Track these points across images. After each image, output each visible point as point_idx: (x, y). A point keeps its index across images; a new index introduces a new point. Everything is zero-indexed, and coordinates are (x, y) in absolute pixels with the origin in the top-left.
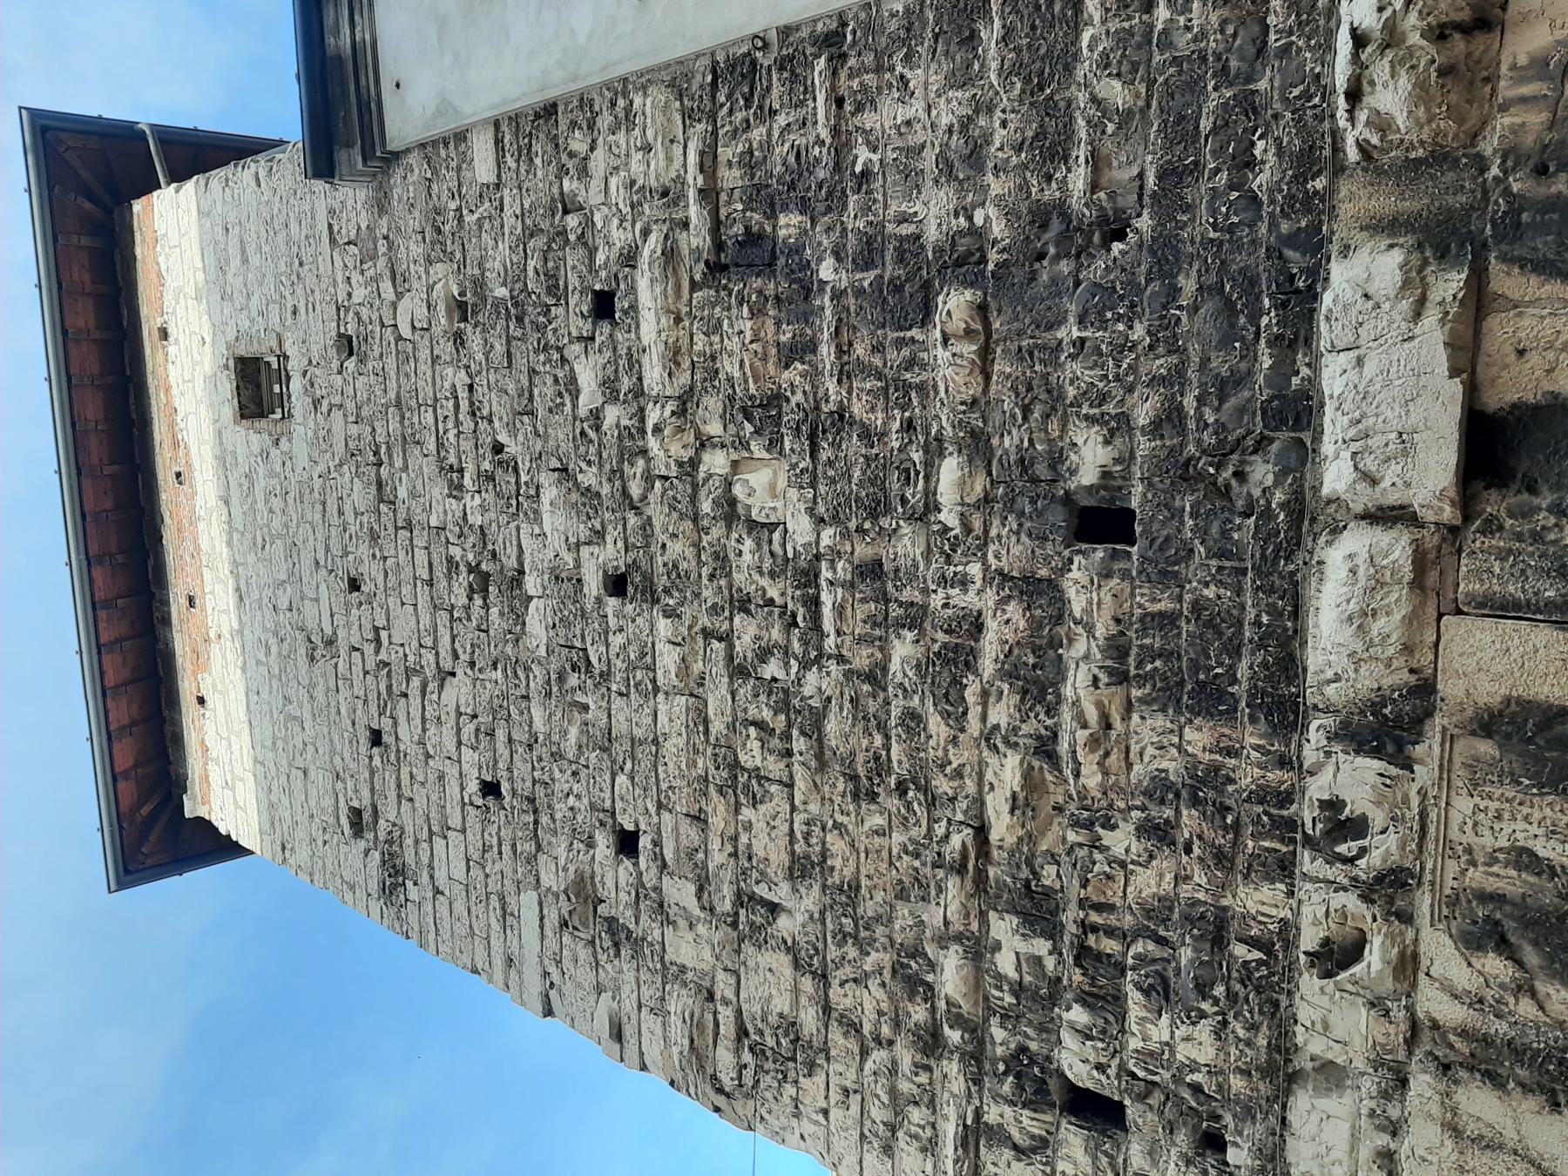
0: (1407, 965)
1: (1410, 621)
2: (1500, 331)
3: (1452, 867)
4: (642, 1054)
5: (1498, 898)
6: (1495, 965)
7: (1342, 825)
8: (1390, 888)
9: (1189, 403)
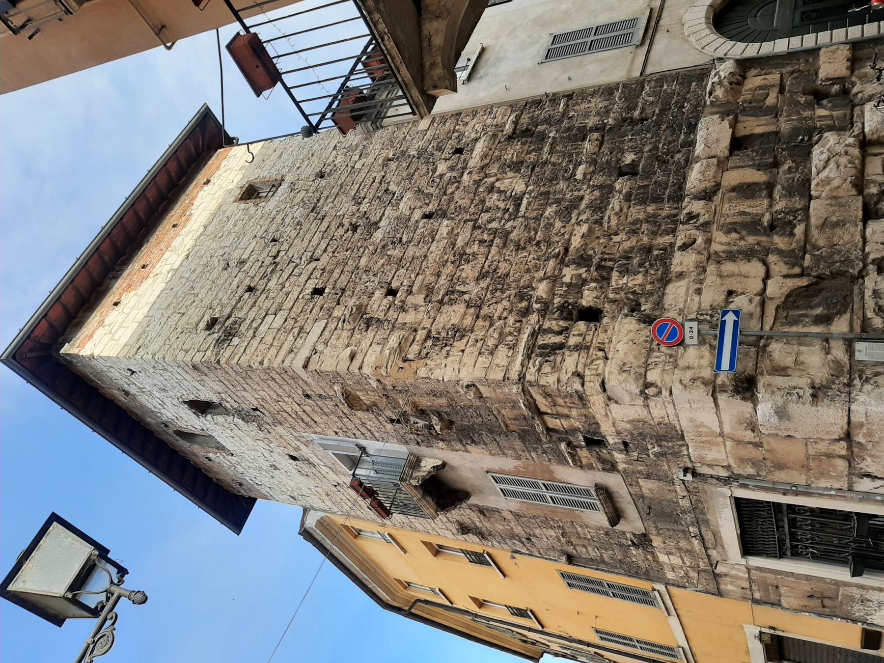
0: (709, 241)
1: (716, 172)
2: (740, 126)
3: (722, 219)
4: (363, 362)
5: (736, 223)
6: (734, 235)
7: (691, 217)
8: (705, 226)
9: (661, 146)
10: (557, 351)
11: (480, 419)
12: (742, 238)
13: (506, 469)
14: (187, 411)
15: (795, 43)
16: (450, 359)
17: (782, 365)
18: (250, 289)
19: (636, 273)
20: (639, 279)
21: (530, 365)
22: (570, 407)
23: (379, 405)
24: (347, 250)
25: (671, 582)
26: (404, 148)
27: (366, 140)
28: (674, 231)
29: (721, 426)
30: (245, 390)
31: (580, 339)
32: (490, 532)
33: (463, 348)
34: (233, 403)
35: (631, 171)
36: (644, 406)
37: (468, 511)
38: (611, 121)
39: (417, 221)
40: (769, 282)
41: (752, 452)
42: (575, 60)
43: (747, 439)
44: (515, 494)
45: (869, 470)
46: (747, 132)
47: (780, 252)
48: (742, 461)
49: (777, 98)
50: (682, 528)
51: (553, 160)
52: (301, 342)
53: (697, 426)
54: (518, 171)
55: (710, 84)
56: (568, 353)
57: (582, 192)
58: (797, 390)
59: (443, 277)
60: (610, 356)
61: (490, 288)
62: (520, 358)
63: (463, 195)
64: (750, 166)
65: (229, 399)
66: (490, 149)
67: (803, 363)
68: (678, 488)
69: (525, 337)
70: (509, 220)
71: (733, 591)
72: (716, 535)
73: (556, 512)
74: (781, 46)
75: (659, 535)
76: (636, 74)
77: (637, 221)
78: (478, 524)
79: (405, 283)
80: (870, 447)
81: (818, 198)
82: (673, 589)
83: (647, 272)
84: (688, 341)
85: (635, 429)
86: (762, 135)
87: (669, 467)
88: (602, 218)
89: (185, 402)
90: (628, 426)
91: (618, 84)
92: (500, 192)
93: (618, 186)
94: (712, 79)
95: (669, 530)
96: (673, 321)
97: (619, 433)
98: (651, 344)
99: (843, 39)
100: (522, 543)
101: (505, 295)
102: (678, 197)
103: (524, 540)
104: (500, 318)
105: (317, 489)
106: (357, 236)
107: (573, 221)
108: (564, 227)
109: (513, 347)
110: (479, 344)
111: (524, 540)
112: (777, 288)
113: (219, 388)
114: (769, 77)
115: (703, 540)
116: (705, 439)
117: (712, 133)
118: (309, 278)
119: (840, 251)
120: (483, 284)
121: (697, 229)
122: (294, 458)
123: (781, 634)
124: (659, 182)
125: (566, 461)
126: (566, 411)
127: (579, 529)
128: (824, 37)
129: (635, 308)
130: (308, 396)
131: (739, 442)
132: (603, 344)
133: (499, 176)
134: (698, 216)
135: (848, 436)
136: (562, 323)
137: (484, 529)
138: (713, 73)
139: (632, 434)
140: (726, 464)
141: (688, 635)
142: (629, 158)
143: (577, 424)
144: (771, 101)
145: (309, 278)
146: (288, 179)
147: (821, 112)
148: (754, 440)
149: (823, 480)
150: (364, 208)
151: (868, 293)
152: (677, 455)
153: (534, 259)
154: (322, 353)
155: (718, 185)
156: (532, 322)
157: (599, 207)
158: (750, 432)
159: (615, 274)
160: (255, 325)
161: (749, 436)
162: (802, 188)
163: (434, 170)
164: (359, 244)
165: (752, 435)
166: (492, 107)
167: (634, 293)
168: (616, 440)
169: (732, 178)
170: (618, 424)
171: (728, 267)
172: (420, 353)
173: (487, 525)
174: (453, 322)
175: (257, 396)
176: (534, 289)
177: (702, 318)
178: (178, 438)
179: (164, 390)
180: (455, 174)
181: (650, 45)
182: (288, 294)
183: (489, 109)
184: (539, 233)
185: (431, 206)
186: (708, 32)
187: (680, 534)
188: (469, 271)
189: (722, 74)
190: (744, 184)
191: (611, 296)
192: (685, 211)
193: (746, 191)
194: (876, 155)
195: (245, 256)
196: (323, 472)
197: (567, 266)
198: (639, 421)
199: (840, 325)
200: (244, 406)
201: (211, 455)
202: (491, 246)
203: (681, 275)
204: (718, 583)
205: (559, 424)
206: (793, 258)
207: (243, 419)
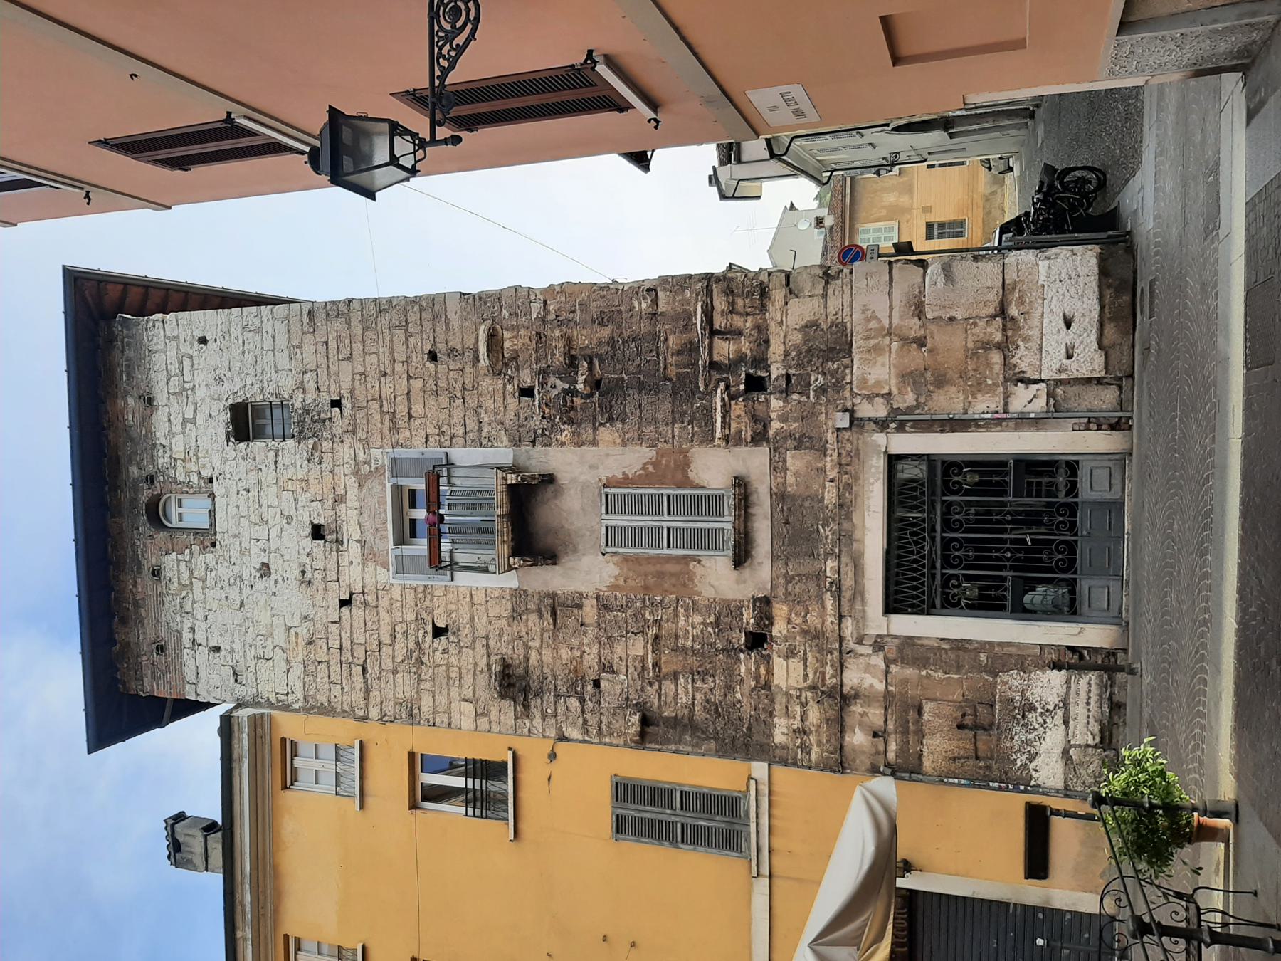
29: (890, 317)
135: (1002, 312)
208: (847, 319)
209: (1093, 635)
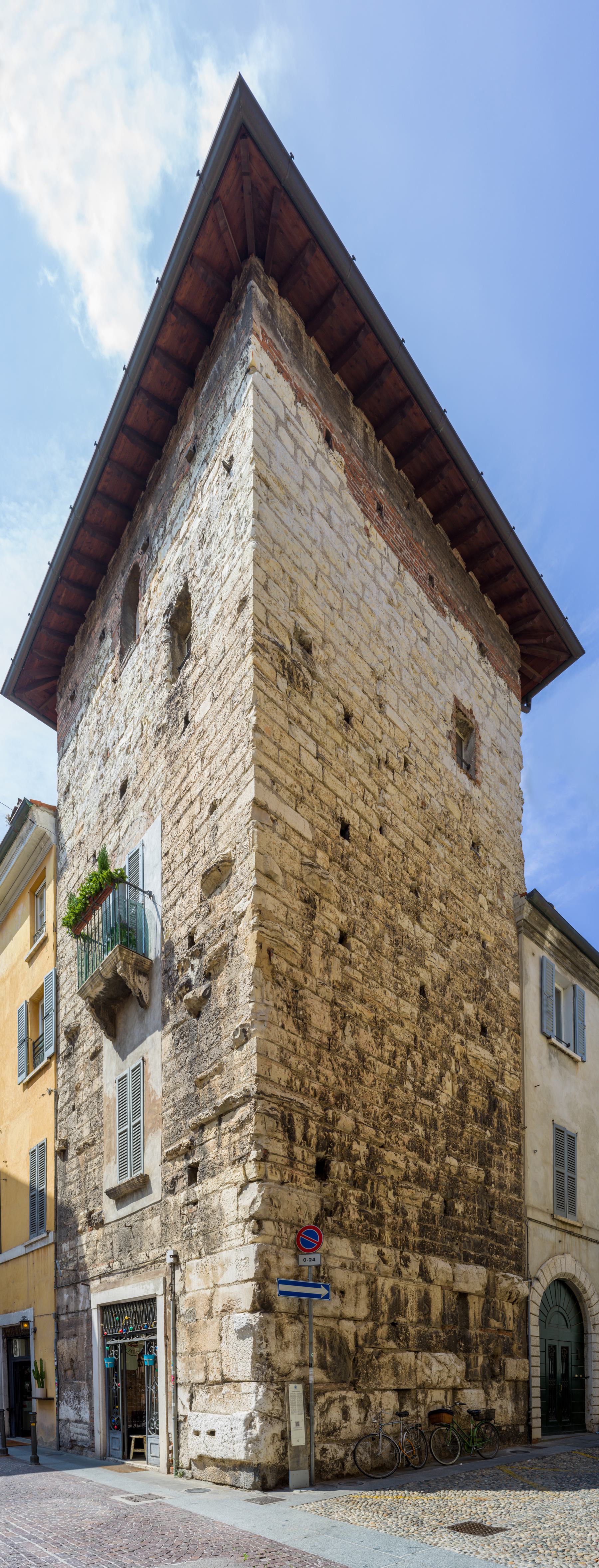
4: (266, 892)
5: (399, 1296)
6: (389, 1295)
7: (406, 1260)
9: (467, 1234)
10: (287, 1134)
11: (205, 1048)
12: (387, 1300)
13: (150, 1081)
14: (173, 590)
15: (535, 1341)
16: (274, 1012)
17: (284, 1332)
18: (348, 717)
19: (360, 1211)
20: (355, 1216)
21: (272, 1105)
22: (229, 1148)
23: (211, 917)
24: (391, 876)
25: (59, 1247)
26: (496, 962)
27: (508, 912)
28: (395, 1245)
29: (224, 1285)
30: (214, 699)
31: (300, 1158)
32: (74, 1065)
33: (286, 1028)
34: (194, 677)
35: (448, 1209)
36: (237, 1219)
37: (93, 1038)
38: (492, 1191)
39: (418, 975)
40: (352, 1323)
41: (201, 1313)
42: (550, 1156)
43: (214, 1306)
44: (122, 1091)
45: (198, 1397)
46: (471, 1304)
47: (375, 1330)
48: (192, 1303)
49: (495, 1327)
50: (116, 1255)
51: (465, 1134)
52: (285, 798)
53: (222, 1265)
54: (459, 1097)
55: (511, 1275)
56: (286, 1145)
57: (433, 1162)
58: (264, 1344)
59: (360, 1007)
60: (284, 1187)
61: (348, 1063)
62: (278, 1093)
63: (441, 1034)
64: (444, 1307)
65: (198, 670)
66: (482, 1067)
67: (287, 1347)
68: (155, 1251)
69: (300, 1099)
70: (414, 1086)
71: (63, 1299)
72: (116, 1284)
73: (110, 1137)
74: (534, 1330)
75: (105, 1236)
76: (530, 1214)
77: (405, 1214)
78: (80, 1051)
79: (353, 954)
80: (219, 1396)
81: (416, 1357)
82: (52, 1249)
83: (361, 1222)
84: (301, 1257)
85: (213, 1211)
86: (467, 1316)
87: (177, 1243)
88: (410, 1181)
89: (186, 585)
90: (214, 1205)
91: (524, 1198)
92: (442, 1076)
93: (436, 1196)
94: (516, 1278)
95: (111, 1244)
96: (320, 1244)
97: (206, 1196)
98: (297, 1226)
99: (533, 1374)
100: (68, 1102)
101: (341, 1079)
102: (423, 1248)
103: (72, 1103)
104: (318, 1072)
105: (85, 828)
106: (406, 891)
107: (409, 1153)
108: (404, 1144)
109: (289, 1086)
110: (290, 1047)
111: (72, 1103)
112: (347, 1328)
113: (214, 651)
114: (511, 1321)
115: (109, 1274)
116: (210, 1272)
117: (473, 1278)
118: (361, 817)
119: (374, 1372)
120: (352, 1054)
121: (397, 1265)
122: (123, 790)
123: (31, 1338)
124: (435, 1235)
125: (169, 1145)
126: (225, 1143)
127: (95, 1160)
128: (536, 1361)
129: (327, 1212)
130: (213, 808)
131: (211, 1300)
132: (296, 1180)
133: (456, 1076)
134: (406, 1266)
135: (225, 1381)
136: (314, 1141)
137: (75, 1058)
138: (521, 1278)
139: (207, 1208)
140: (187, 1289)
141: (10, 1263)
142: (460, 1207)
143: (212, 1155)
144: (494, 1323)
145: (361, 817)
146: (476, 792)
147: (481, 1360)
148: (214, 1311)
149: (184, 1365)
150: (437, 905)
151: (343, 1393)
152: (190, 1248)
153: (376, 1112)
154: (274, 830)
155: (431, 1282)
156: (315, 1108)
157: (420, 1178)
158: (221, 1308)
159: (358, 1193)
160: (304, 721)
161: (218, 1307)
162: (425, 1345)
163: (468, 999)
164: (397, 894)
165: (219, 1310)
166: (522, 1071)
167: (343, 1211)
168: (198, 1194)
169: (436, 1296)
170: (217, 1195)
171: (364, 1291)
172: (278, 972)
173: (81, 1062)
174: (313, 1016)
175: (207, 723)
176: (347, 1111)
177: (321, 1269)
178: (128, 573)
179: (202, 540)
180: (462, 1024)
181: (551, 1226)
182: (341, 778)
183: (520, 1067)
184: (399, 1118)
185: (432, 993)
186: (554, 1275)
187: (109, 1254)
188: (366, 1037)
189: (519, 1286)
190: (430, 1302)
191: (340, 1189)
192: (410, 1255)
193: (425, 1303)
194: (446, 1397)
195: (389, 711)
196: (111, 835)
197: (368, 1146)
198: (221, 1214)
199: (315, 1375)
200: (190, 700)
201: (108, 642)
202: (389, 1064)
203: (357, 1253)
204: (67, 1286)
205: (209, 1137)
206: (371, 1338)
207: (170, 699)
208: (224, 1247)
209: (537, 1433)
